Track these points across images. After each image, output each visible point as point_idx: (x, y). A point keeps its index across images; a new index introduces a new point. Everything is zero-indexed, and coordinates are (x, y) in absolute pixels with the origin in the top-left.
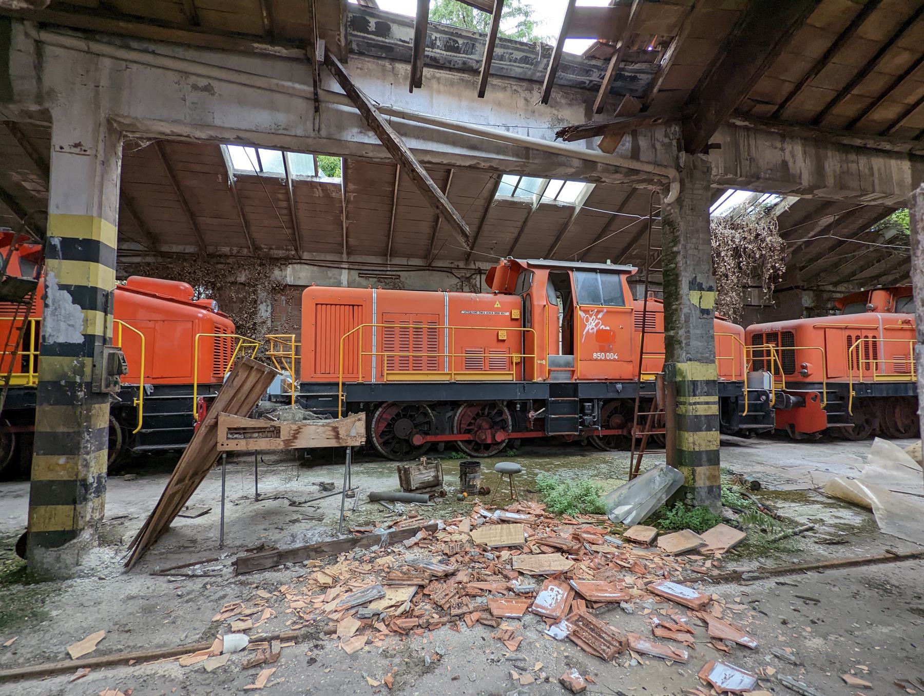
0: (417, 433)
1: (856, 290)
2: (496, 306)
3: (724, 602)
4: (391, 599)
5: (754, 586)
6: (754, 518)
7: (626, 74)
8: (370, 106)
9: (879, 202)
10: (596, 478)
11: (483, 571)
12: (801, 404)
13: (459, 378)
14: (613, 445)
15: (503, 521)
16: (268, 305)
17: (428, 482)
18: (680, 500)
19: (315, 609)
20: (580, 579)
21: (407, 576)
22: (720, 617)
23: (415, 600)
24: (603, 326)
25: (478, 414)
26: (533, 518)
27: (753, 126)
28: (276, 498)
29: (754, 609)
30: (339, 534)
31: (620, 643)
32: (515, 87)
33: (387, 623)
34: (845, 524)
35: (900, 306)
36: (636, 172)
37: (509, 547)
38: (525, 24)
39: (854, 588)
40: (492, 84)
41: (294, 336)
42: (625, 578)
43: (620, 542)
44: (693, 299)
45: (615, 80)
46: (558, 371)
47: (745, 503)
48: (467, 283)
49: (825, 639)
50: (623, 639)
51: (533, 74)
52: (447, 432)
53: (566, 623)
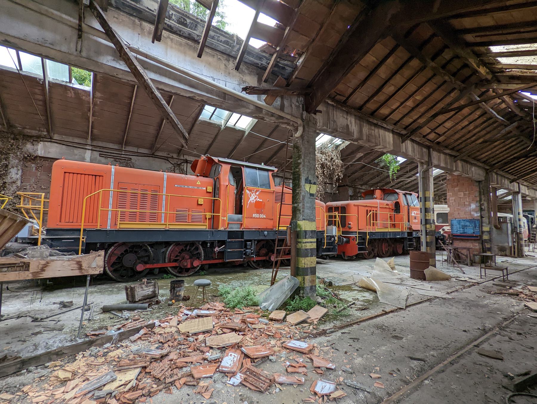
0: (140, 263)
1: (369, 189)
2: (198, 183)
3: (319, 347)
4: (121, 380)
5: (332, 336)
6: (331, 301)
7: (280, 65)
8: (123, 44)
9: (382, 150)
10: (252, 285)
11: (187, 350)
12: (348, 242)
13: (171, 227)
14: (261, 266)
15: (199, 316)
16: (18, 170)
17: (148, 295)
18: (297, 295)
19: (56, 399)
20: (246, 346)
21: (133, 362)
22: (318, 355)
23: (139, 377)
24: (259, 199)
25: (182, 250)
26: (218, 312)
27: (335, 105)
28: (18, 317)
29: (333, 348)
30: (77, 339)
31: (270, 380)
32: (219, 57)
33: (117, 398)
34: (367, 300)
35: (385, 197)
36: (282, 118)
37: (203, 332)
38: (221, 23)
39: (372, 330)
40: (206, 52)
41: (44, 194)
42: (271, 342)
43: (267, 321)
44: (307, 188)
45: (275, 67)
46: (233, 224)
47: (327, 293)
48: (178, 167)
49: (362, 358)
50: (272, 378)
51: (231, 52)
52: (161, 262)
53: (240, 374)
